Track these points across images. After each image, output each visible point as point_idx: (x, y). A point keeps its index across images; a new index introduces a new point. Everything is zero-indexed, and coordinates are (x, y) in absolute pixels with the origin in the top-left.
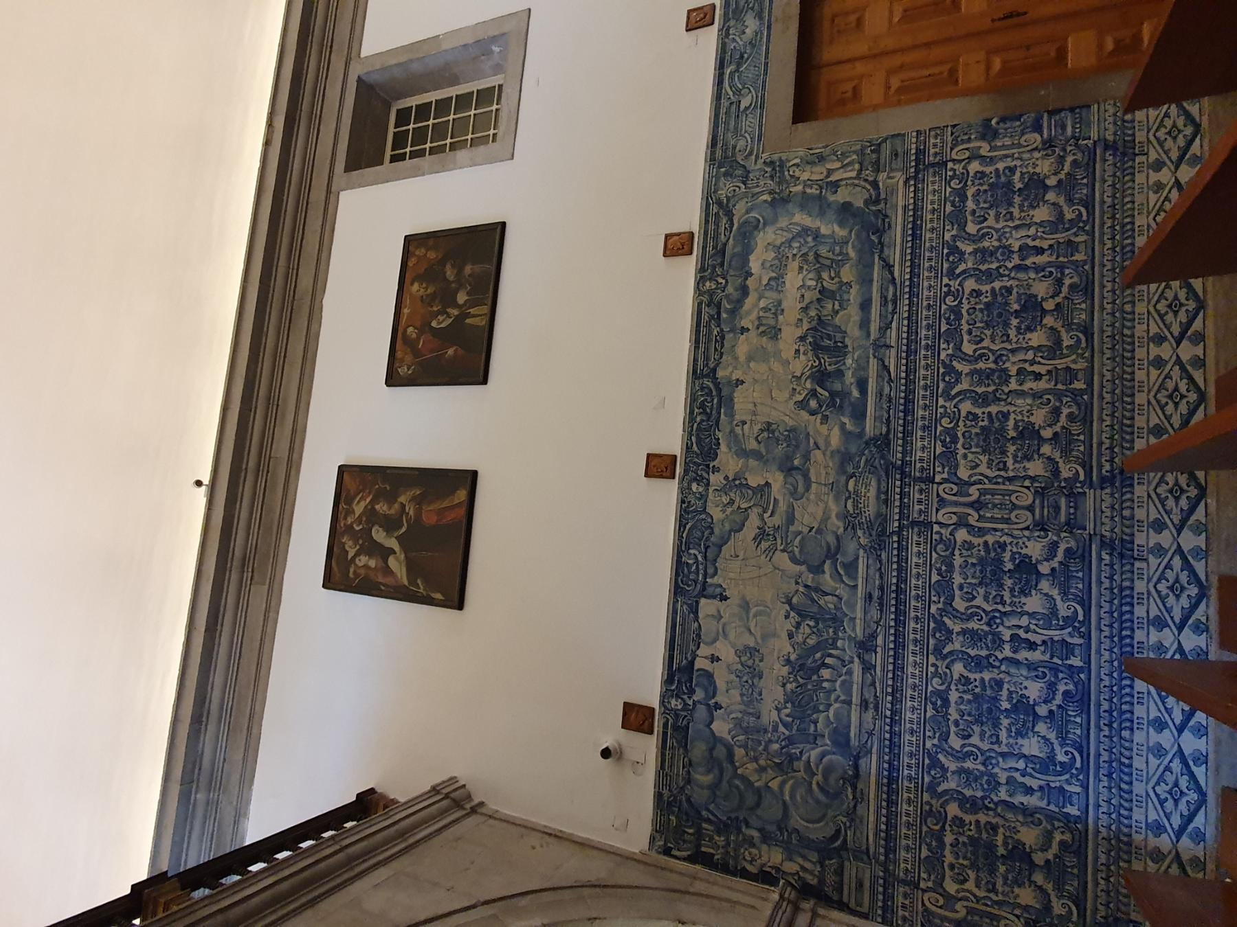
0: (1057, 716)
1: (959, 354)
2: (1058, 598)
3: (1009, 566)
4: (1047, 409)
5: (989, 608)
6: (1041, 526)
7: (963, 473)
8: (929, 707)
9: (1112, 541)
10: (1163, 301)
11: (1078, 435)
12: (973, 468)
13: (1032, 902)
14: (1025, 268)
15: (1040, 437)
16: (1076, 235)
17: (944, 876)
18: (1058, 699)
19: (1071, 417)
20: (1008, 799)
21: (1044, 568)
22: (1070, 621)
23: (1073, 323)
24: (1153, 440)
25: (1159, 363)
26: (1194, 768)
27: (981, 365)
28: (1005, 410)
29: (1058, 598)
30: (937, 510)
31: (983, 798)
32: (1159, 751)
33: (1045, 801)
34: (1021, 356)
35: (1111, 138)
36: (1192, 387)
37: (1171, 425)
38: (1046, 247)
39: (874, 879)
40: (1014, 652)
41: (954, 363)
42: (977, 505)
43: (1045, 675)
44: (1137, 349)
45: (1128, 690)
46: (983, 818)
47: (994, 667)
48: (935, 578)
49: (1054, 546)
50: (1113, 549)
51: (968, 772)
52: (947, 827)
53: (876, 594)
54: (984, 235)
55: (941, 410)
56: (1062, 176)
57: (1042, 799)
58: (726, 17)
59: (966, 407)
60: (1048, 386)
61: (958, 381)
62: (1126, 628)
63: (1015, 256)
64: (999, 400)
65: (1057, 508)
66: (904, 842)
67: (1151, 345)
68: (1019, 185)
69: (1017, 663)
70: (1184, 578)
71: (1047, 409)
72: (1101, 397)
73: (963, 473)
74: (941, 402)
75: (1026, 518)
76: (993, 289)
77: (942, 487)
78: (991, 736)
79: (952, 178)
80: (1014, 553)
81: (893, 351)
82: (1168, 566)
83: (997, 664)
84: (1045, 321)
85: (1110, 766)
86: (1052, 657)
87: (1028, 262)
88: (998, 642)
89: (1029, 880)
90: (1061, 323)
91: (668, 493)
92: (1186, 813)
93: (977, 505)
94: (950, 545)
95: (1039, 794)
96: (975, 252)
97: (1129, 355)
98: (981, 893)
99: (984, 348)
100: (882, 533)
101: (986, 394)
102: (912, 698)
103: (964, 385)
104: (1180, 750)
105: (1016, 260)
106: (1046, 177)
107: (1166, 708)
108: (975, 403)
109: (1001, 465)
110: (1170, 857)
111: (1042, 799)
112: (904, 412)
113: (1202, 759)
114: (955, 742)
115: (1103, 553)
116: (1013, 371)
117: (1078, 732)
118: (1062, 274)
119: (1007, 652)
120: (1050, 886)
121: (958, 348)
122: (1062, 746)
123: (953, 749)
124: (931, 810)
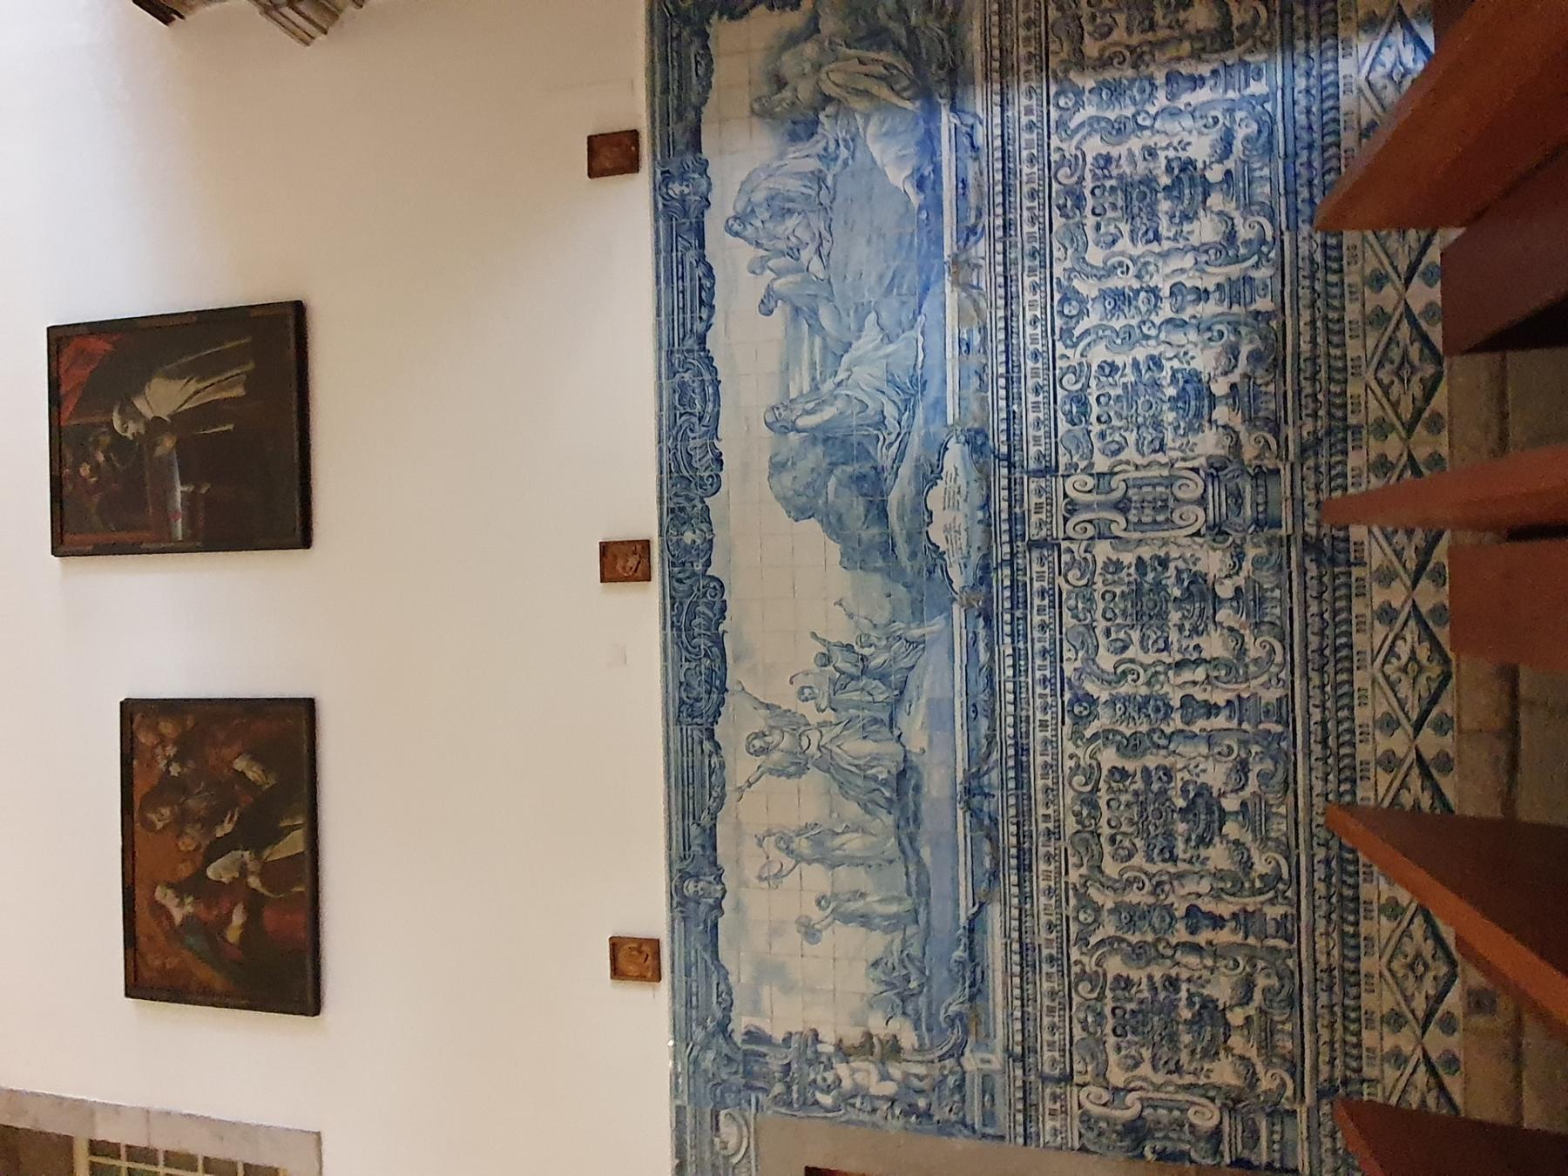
0: (1243, 389)
1: (1082, 268)
2: (1236, 215)
3: (1186, 1014)
4: (1217, 346)
5: (1152, 868)
8: (1056, 212)
9: (1319, 540)
10: (1388, 366)
11: (1272, 590)
12: (1105, 36)
13: (1225, 864)
14: (1175, 114)
15: (1227, 1024)
16: (1256, 266)
17: (1101, 855)
18: (1253, 785)
19: (1255, 357)
20: (1190, 938)
21: (1225, 590)
22: (1271, 881)
23: (1268, 839)
24: (1375, 483)
25: (1380, 317)
26: (1435, 629)
27: (1125, 689)
28: (1167, 762)
29: (1236, 215)
30: (1066, 520)
31: (1155, 944)
32: (1398, 1058)
33: (1241, 934)
34: (1187, 675)
35: (1312, 531)
36: (1440, 954)
37: (1413, 1012)
38: (1222, 703)
40: (1188, 724)
41: (1076, 283)
42: (1122, 506)
43: (1221, 334)
44: (1363, 958)
45: (1346, 688)
46: (1151, 761)
47: (1158, 747)
48: (1078, 1033)
49: (1243, 767)
50: (1321, 551)
51: (1132, 908)
52: (1108, 992)
53: (976, 339)
54: (1129, 883)
55: (1075, 969)
56: (1251, 1010)
57: (1230, 718)
58: (667, 146)
59: (1115, 965)
60: (1219, 310)
61: (1083, 313)
62: (1340, 598)
63: (1177, 716)
64: (1147, 337)
65: (1237, 496)
66: (1045, 952)
67: (1386, 1066)
68: (1165, 180)
69: (1196, 949)
70: (1428, 948)
71: (1217, 346)
72: (1312, 891)
73: (1117, 1077)
74: (1075, 954)
75: (1197, 517)
76: (1134, 360)
77: (1069, 481)
78: (1155, 641)
79: (1070, 567)
80: (1186, 783)
81: (984, 271)
82: (1406, 933)
83: (1153, 332)
84: (1220, 617)
85: (1324, 693)
86: (1240, 723)
87: (1196, 729)
89: (1210, 421)
90: (1233, 204)
91: (652, 1007)
92: (1432, 992)
93: (1122, 506)
94: (1086, 566)
95: (1212, 82)
96: (1103, 295)
97: (1354, 1040)
98: (1159, 1078)
99: (1115, 44)
100: (986, 568)
101: (1142, 945)
102: (1037, 439)
103: (1103, 720)
104: (1419, 757)
105: (1166, 311)
106: (1222, 794)
107: (1398, 700)
108: (1127, 959)
109: (1161, 644)
110: (1407, 609)
111: (1230, 718)
112: (1012, 635)
113: (1445, 763)
114: (1106, 660)
115: (1307, 560)
116: (1180, 911)
117: (1289, 1045)
118: (1233, 120)
119: (1181, 934)
120: (1250, 837)
121: (1091, 659)
122: (1262, 852)
123: (1109, 878)
124: (1078, 766)
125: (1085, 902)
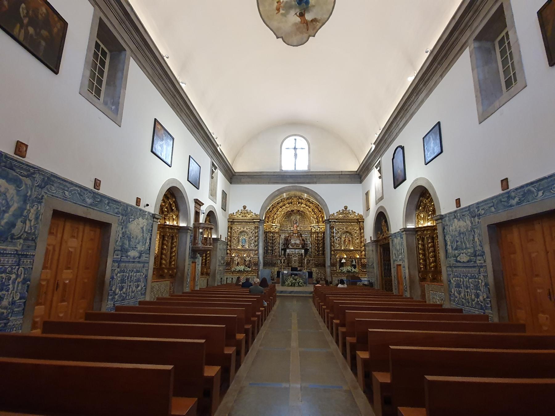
6: (484, 299)
7: (119, 275)
28: (10, 291)
39: (118, 258)
59: (127, 275)
73: (119, 275)
88: (467, 289)
125: (467, 276)
